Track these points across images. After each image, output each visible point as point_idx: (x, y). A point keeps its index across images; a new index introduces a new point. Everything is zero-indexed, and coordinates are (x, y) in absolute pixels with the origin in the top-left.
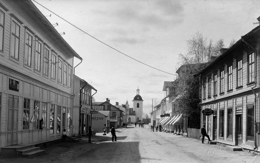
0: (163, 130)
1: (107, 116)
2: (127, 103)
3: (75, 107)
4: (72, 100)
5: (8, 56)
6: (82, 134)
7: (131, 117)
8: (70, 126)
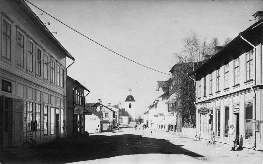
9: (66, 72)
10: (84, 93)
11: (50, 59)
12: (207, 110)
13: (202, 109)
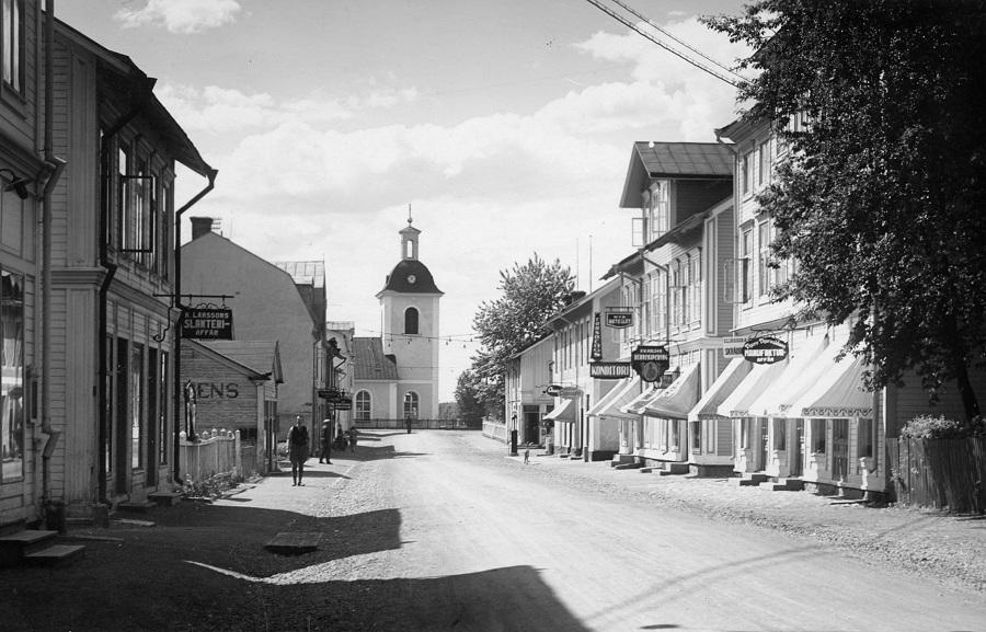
1: (266, 377)
3: (70, 277)
6: (118, 499)
8: (27, 435)
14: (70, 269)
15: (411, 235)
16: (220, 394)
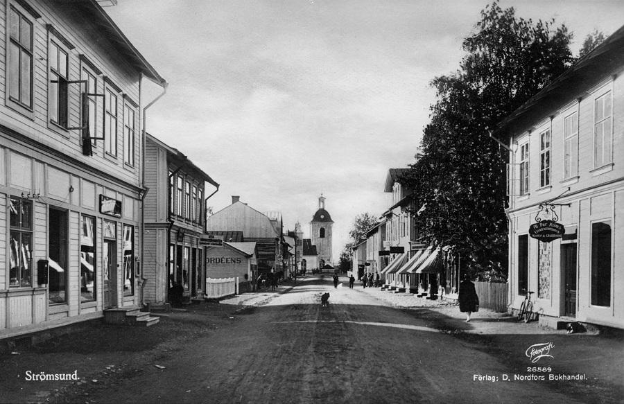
0: (387, 287)
1: (251, 256)
2: (297, 226)
4: (141, 203)
5: (45, 119)
7: (308, 258)
9: (142, 121)
10: (204, 189)
11: (122, 103)
12: (557, 226)
13: (541, 224)
14: (158, 222)
15: (321, 200)
16: (234, 262)
